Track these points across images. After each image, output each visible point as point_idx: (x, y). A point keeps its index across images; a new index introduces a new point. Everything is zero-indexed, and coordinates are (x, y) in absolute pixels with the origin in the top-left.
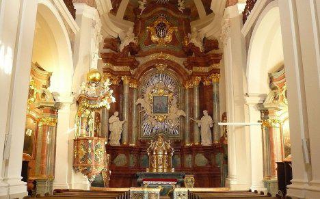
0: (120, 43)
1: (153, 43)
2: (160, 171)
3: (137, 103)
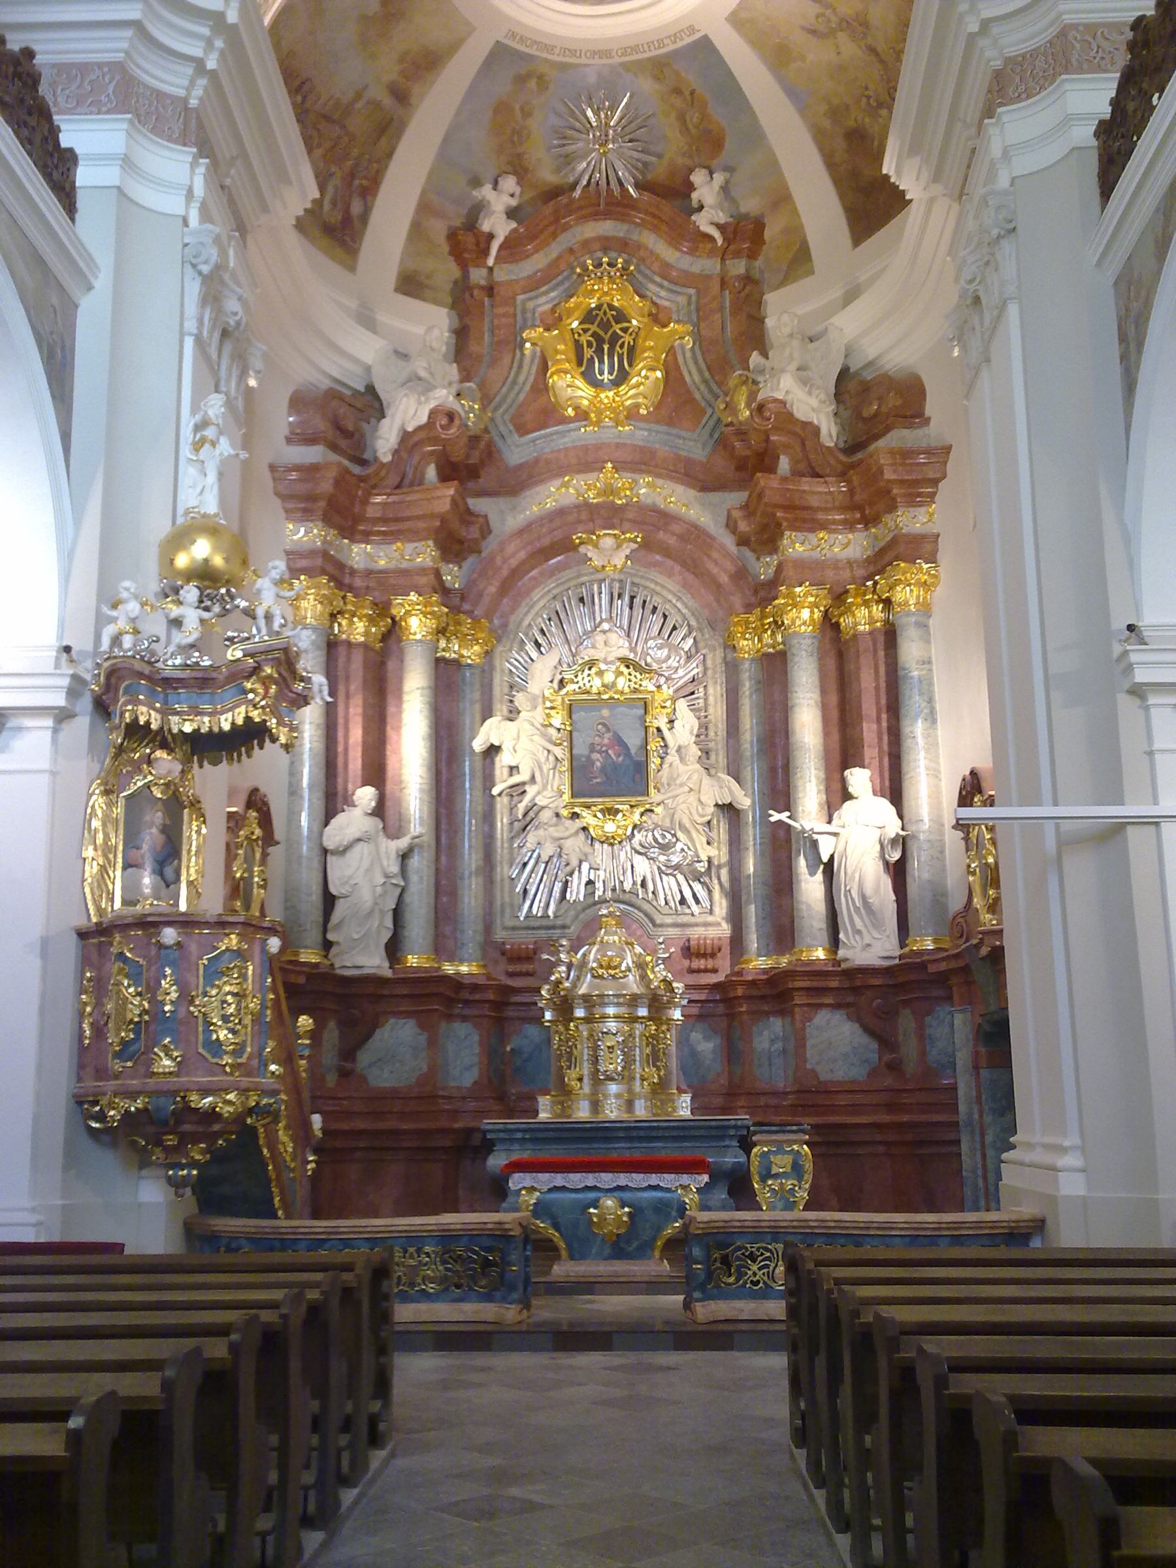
0: (382, 415)
1: (565, 420)
2: (612, 1111)
3: (478, 745)
